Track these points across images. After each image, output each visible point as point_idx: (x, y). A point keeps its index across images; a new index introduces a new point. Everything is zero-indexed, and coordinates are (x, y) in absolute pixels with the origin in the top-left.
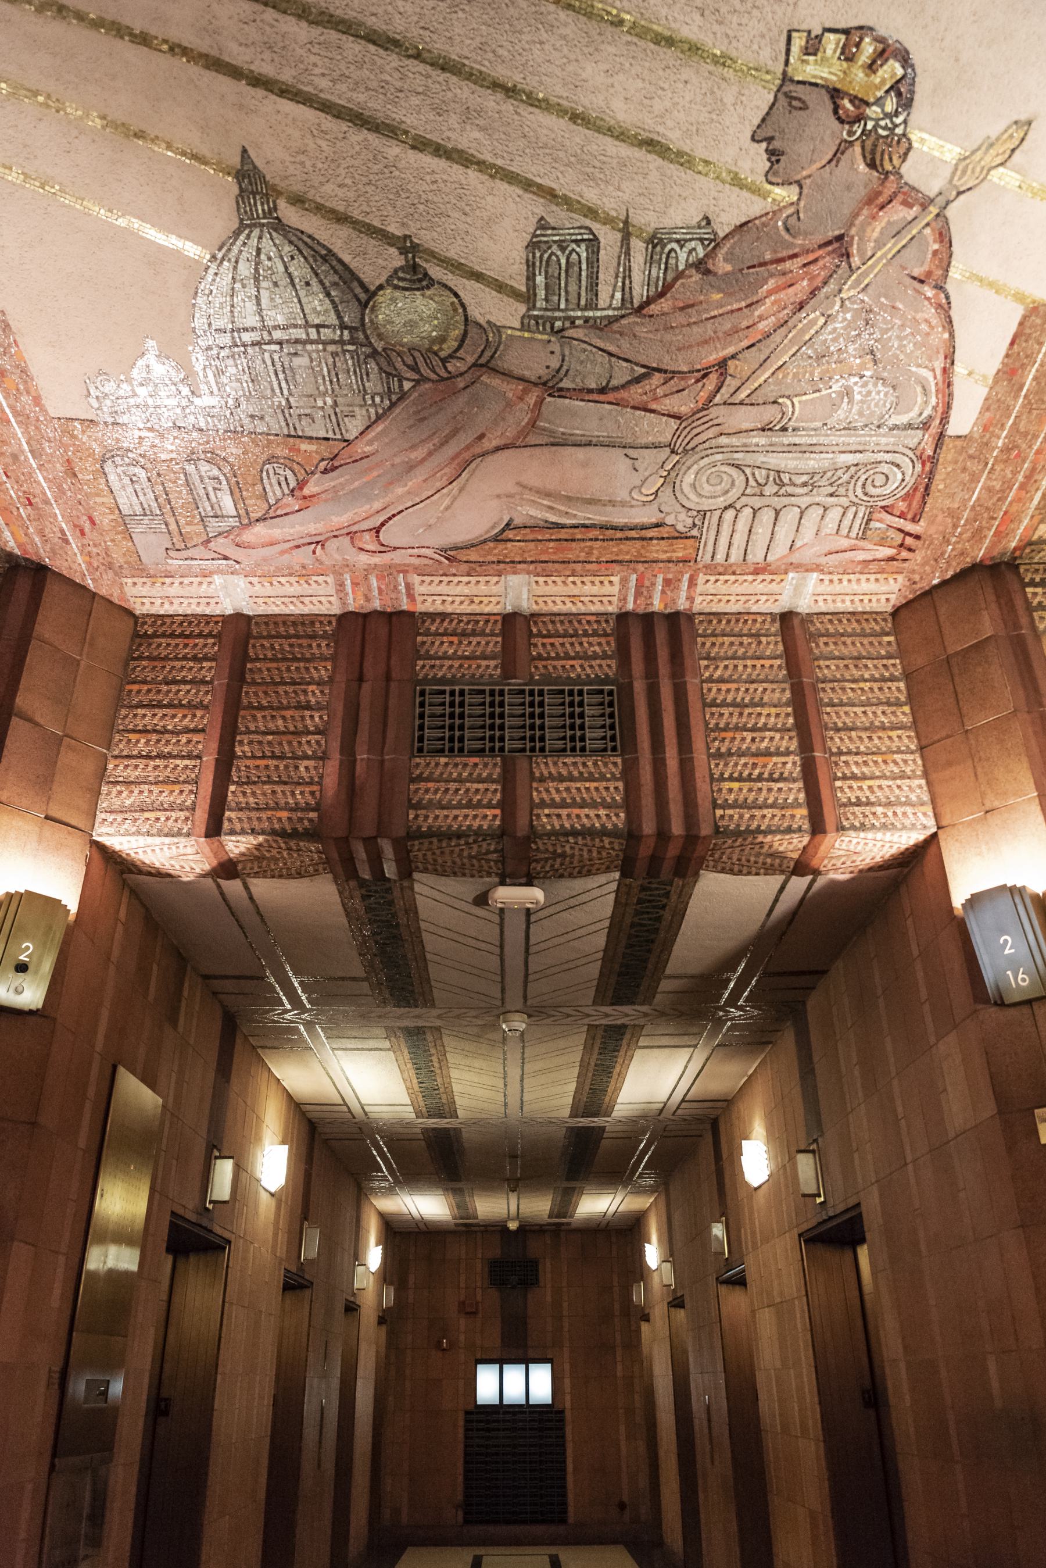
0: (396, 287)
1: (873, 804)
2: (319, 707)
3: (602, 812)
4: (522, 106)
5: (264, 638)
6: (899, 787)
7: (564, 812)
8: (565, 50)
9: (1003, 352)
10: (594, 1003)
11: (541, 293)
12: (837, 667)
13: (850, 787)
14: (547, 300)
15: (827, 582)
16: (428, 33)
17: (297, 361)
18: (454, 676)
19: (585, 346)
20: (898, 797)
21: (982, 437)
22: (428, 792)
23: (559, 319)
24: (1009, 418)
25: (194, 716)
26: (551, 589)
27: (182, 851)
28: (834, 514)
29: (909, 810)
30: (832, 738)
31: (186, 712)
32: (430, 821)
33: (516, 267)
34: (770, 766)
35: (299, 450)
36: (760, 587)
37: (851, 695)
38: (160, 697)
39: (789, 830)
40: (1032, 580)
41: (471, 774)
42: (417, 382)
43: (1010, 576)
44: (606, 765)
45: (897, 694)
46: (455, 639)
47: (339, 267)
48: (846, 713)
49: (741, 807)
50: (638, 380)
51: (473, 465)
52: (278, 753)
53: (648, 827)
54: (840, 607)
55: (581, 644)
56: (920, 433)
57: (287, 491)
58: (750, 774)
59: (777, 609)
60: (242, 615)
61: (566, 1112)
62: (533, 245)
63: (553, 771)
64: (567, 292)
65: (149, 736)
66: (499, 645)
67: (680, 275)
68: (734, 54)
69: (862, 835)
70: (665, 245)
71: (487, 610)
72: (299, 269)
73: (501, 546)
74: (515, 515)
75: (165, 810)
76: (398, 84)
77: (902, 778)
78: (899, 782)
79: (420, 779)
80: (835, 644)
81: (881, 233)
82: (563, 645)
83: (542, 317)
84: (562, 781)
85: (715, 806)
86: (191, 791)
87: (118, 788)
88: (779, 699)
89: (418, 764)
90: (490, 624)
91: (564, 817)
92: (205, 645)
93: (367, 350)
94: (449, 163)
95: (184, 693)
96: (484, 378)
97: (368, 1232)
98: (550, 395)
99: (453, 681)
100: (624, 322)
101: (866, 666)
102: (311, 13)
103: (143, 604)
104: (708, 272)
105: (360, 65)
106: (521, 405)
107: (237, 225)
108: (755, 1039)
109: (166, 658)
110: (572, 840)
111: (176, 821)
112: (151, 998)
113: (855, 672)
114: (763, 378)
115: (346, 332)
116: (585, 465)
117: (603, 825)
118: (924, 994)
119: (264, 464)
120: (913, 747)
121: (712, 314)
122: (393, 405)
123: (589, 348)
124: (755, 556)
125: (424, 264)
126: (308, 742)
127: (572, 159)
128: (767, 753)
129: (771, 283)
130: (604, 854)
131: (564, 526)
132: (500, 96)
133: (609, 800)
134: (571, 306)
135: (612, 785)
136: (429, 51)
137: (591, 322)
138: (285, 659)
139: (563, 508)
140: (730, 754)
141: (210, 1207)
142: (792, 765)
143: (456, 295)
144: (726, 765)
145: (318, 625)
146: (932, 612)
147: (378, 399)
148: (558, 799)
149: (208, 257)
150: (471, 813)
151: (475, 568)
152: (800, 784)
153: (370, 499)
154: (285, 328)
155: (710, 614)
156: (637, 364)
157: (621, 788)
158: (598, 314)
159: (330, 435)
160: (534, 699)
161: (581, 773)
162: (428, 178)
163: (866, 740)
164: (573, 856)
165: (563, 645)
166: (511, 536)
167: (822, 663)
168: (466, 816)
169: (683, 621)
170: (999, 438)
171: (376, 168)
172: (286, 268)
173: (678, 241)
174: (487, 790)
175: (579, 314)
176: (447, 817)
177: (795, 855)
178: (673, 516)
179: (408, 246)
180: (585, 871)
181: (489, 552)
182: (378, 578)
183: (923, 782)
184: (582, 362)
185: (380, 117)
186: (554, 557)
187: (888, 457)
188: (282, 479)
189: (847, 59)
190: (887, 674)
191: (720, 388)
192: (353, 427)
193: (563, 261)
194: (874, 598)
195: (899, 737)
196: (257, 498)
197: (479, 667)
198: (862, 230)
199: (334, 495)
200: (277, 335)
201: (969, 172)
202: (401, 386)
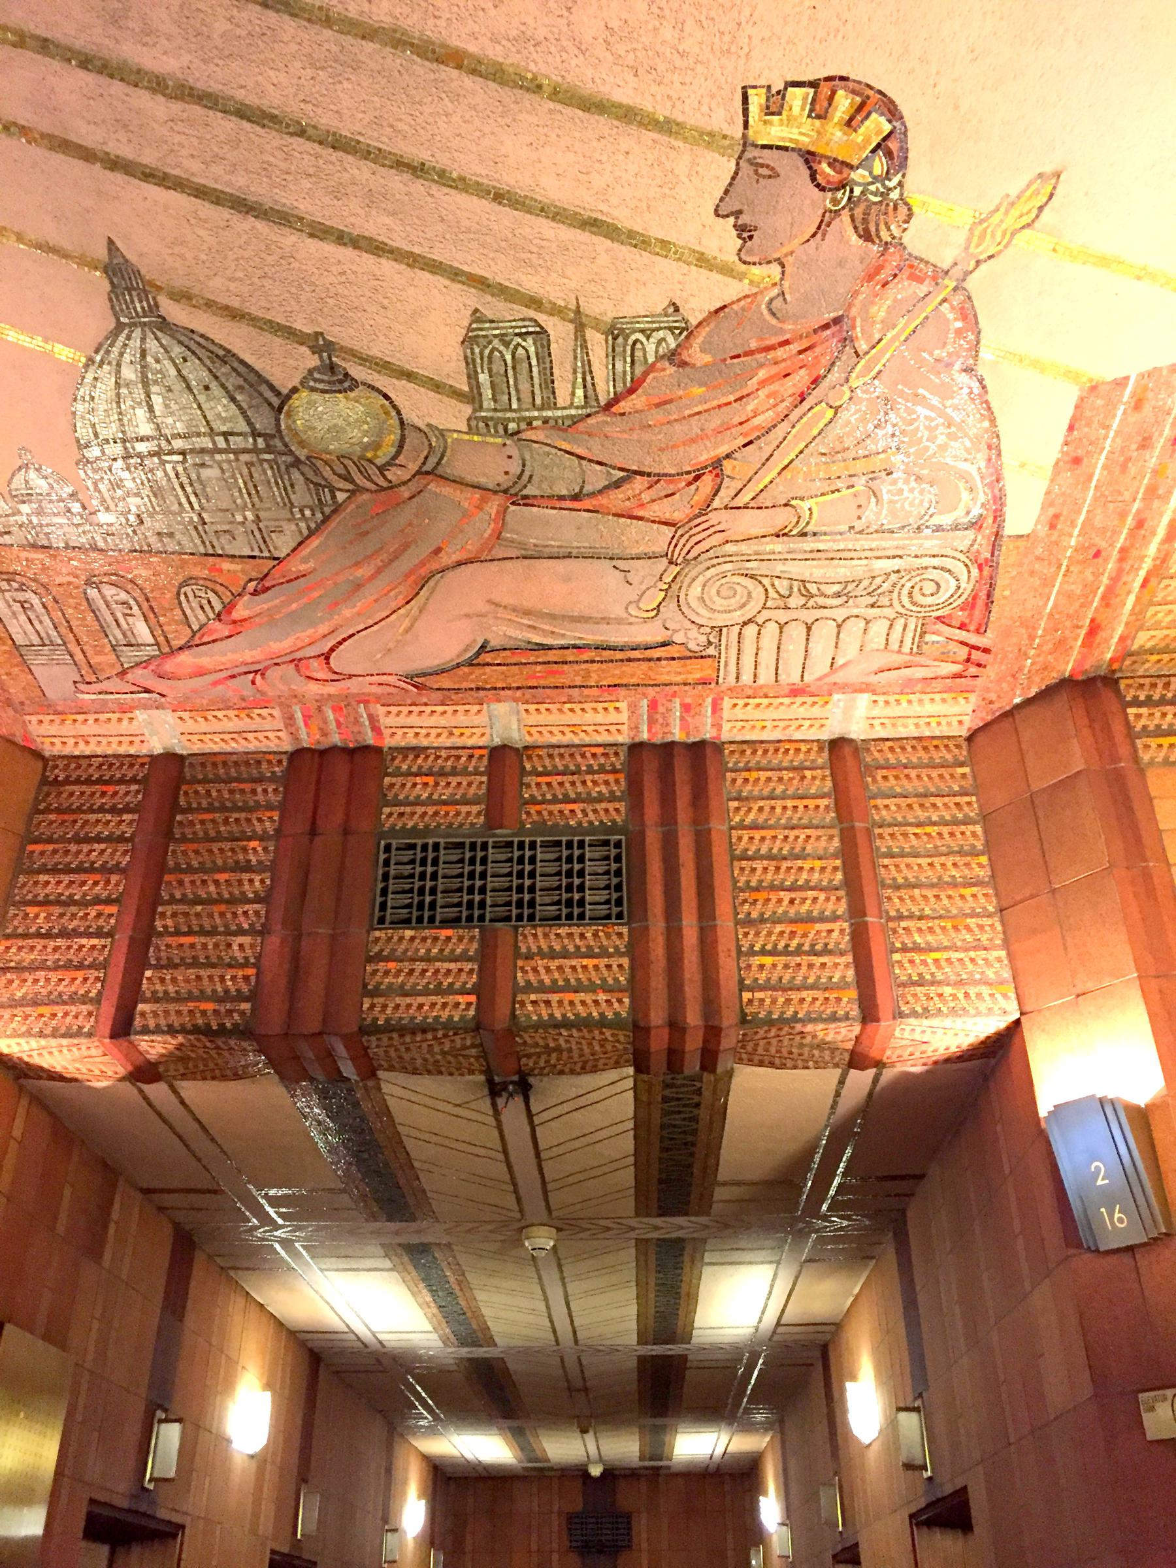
0: (313, 389)
1: (939, 983)
2: (260, 868)
3: (602, 997)
4: (435, 187)
5: (199, 782)
6: (972, 960)
7: (554, 998)
8: (477, 122)
9: (1061, 440)
10: (637, 1215)
11: (488, 393)
12: (898, 806)
13: (912, 962)
14: (495, 399)
15: (881, 704)
16: (310, 107)
17: (206, 473)
18: (427, 826)
19: (547, 449)
20: (971, 973)
21: (1049, 536)
22: (387, 974)
23: (513, 420)
24: (1079, 513)
25: (108, 882)
26: (543, 718)
27: (85, 1053)
28: (879, 629)
29: (985, 991)
30: (889, 898)
31: (97, 877)
32: (389, 1011)
33: (453, 364)
34: (811, 936)
35: (220, 570)
36: (802, 712)
37: (914, 841)
38: (68, 859)
39: (834, 1018)
40: (1136, 698)
41: (442, 950)
42: (353, 493)
43: (1107, 694)
44: (608, 936)
45: (972, 841)
46: (430, 780)
47: (241, 369)
48: (908, 866)
49: (774, 989)
50: (617, 484)
51: (431, 583)
52: (208, 927)
53: (657, 1017)
54: (902, 732)
55: (584, 783)
56: (971, 534)
57: (212, 616)
58: (787, 946)
59: (825, 736)
60: (175, 755)
61: (632, 1339)
62: (469, 340)
63: (544, 947)
64: (517, 391)
65: (51, 909)
66: (484, 786)
67: (652, 368)
68: (680, 119)
69: (926, 1022)
70: (626, 338)
71: (470, 742)
72: (196, 373)
73: (478, 671)
74: (489, 637)
75: (65, 1003)
76: (283, 165)
77: (975, 948)
78: (972, 954)
79: (379, 957)
80: (897, 778)
81: (888, 312)
82: (561, 784)
83: (492, 419)
84: (553, 958)
85: (742, 987)
86: (97, 979)
87: (9, 976)
88: (826, 849)
89: (378, 939)
90: (474, 761)
91: (554, 1004)
92: (127, 793)
93: (289, 459)
94: (356, 252)
95: (97, 854)
96: (432, 486)
97: (405, 1482)
98: (513, 503)
99: (427, 831)
100: (590, 421)
101: (934, 805)
102: (167, 87)
103: (52, 744)
104: (683, 364)
105: (235, 144)
106: (481, 514)
107: (113, 325)
108: (855, 1252)
109: (80, 810)
110: (565, 1033)
111: (76, 1017)
112: (61, 1228)
113: (919, 813)
114: (768, 479)
115: (260, 440)
116: (567, 579)
117: (602, 1014)
118: (1017, 1226)
119: (181, 586)
120: (991, 909)
121: (696, 410)
122: (326, 519)
123: (554, 451)
124: (789, 675)
125: (343, 364)
126: (245, 913)
127: (503, 244)
128: (809, 919)
129: (762, 374)
130: (609, 1048)
131: (550, 648)
132: (407, 177)
133: (611, 981)
134: (524, 406)
135: (614, 962)
136: (315, 127)
137: (552, 423)
138: (223, 809)
139: (547, 627)
140: (762, 920)
141: (151, 1487)
142: (839, 934)
143: (386, 397)
144: (757, 934)
145: (264, 766)
146: (1014, 738)
147: (308, 513)
148: (547, 981)
149: (84, 360)
150: (440, 1000)
151: (448, 696)
152: (849, 958)
153: (313, 624)
154: (185, 437)
155: (744, 742)
156: (614, 468)
157: (626, 966)
158: (559, 413)
159: (256, 553)
160: (521, 852)
161: (578, 948)
162: (333, 269)
163: (933, 900)
164: (570, 1050)
165: (561, 784)
166: (489, 660)
167: (880, 802)
168: (433, 1005)
169: (709, 752)
170: (1071, 536)
171: (270, 259)
172: (179, 371)
173: (642, 331)
174: (461, 970)
175: (536, 414)
176: (409, 1006)
177: (849, 1046)
178: (682, 633)
179: (320, 344)
180: (590, 1067)
181: (465, 677)
182: (334, 709)
183: (1003, 954)
184: (546, 467)
185: (268, 203)
186: (542, 682)
187: (936, 562)
188: (204, 602)
189: (818, 117)
190: (960, 816)
191: (717, 491)
192: (283, 544)
193: (508, 357)
194: (944, 721)
195: (974, 896)
196: (177, 623)
197: (458, 814)
198: (865, 308)
199: (270, 619)
200: (178, 444)
201: (988, 237)
202: (334, 497)
